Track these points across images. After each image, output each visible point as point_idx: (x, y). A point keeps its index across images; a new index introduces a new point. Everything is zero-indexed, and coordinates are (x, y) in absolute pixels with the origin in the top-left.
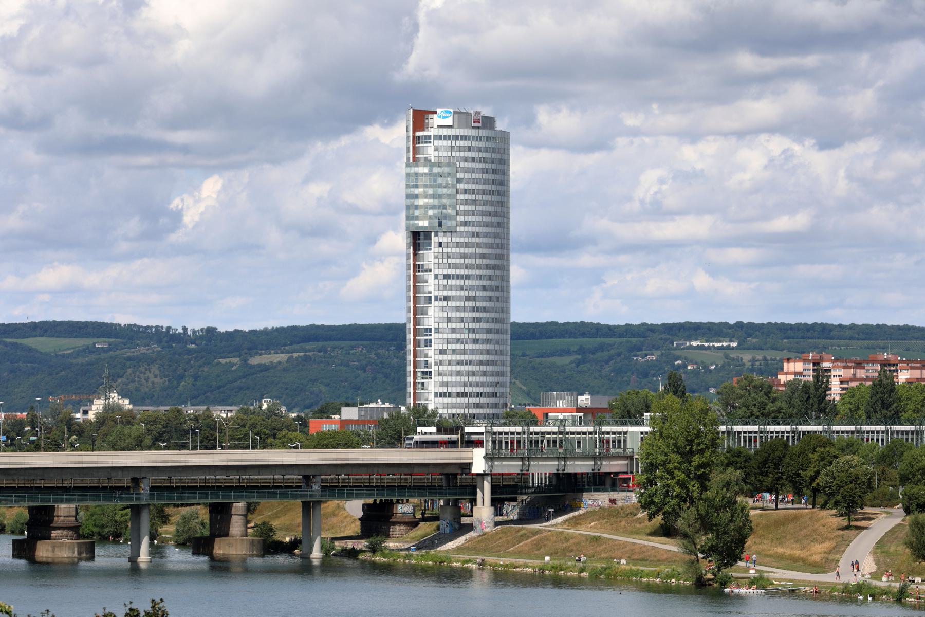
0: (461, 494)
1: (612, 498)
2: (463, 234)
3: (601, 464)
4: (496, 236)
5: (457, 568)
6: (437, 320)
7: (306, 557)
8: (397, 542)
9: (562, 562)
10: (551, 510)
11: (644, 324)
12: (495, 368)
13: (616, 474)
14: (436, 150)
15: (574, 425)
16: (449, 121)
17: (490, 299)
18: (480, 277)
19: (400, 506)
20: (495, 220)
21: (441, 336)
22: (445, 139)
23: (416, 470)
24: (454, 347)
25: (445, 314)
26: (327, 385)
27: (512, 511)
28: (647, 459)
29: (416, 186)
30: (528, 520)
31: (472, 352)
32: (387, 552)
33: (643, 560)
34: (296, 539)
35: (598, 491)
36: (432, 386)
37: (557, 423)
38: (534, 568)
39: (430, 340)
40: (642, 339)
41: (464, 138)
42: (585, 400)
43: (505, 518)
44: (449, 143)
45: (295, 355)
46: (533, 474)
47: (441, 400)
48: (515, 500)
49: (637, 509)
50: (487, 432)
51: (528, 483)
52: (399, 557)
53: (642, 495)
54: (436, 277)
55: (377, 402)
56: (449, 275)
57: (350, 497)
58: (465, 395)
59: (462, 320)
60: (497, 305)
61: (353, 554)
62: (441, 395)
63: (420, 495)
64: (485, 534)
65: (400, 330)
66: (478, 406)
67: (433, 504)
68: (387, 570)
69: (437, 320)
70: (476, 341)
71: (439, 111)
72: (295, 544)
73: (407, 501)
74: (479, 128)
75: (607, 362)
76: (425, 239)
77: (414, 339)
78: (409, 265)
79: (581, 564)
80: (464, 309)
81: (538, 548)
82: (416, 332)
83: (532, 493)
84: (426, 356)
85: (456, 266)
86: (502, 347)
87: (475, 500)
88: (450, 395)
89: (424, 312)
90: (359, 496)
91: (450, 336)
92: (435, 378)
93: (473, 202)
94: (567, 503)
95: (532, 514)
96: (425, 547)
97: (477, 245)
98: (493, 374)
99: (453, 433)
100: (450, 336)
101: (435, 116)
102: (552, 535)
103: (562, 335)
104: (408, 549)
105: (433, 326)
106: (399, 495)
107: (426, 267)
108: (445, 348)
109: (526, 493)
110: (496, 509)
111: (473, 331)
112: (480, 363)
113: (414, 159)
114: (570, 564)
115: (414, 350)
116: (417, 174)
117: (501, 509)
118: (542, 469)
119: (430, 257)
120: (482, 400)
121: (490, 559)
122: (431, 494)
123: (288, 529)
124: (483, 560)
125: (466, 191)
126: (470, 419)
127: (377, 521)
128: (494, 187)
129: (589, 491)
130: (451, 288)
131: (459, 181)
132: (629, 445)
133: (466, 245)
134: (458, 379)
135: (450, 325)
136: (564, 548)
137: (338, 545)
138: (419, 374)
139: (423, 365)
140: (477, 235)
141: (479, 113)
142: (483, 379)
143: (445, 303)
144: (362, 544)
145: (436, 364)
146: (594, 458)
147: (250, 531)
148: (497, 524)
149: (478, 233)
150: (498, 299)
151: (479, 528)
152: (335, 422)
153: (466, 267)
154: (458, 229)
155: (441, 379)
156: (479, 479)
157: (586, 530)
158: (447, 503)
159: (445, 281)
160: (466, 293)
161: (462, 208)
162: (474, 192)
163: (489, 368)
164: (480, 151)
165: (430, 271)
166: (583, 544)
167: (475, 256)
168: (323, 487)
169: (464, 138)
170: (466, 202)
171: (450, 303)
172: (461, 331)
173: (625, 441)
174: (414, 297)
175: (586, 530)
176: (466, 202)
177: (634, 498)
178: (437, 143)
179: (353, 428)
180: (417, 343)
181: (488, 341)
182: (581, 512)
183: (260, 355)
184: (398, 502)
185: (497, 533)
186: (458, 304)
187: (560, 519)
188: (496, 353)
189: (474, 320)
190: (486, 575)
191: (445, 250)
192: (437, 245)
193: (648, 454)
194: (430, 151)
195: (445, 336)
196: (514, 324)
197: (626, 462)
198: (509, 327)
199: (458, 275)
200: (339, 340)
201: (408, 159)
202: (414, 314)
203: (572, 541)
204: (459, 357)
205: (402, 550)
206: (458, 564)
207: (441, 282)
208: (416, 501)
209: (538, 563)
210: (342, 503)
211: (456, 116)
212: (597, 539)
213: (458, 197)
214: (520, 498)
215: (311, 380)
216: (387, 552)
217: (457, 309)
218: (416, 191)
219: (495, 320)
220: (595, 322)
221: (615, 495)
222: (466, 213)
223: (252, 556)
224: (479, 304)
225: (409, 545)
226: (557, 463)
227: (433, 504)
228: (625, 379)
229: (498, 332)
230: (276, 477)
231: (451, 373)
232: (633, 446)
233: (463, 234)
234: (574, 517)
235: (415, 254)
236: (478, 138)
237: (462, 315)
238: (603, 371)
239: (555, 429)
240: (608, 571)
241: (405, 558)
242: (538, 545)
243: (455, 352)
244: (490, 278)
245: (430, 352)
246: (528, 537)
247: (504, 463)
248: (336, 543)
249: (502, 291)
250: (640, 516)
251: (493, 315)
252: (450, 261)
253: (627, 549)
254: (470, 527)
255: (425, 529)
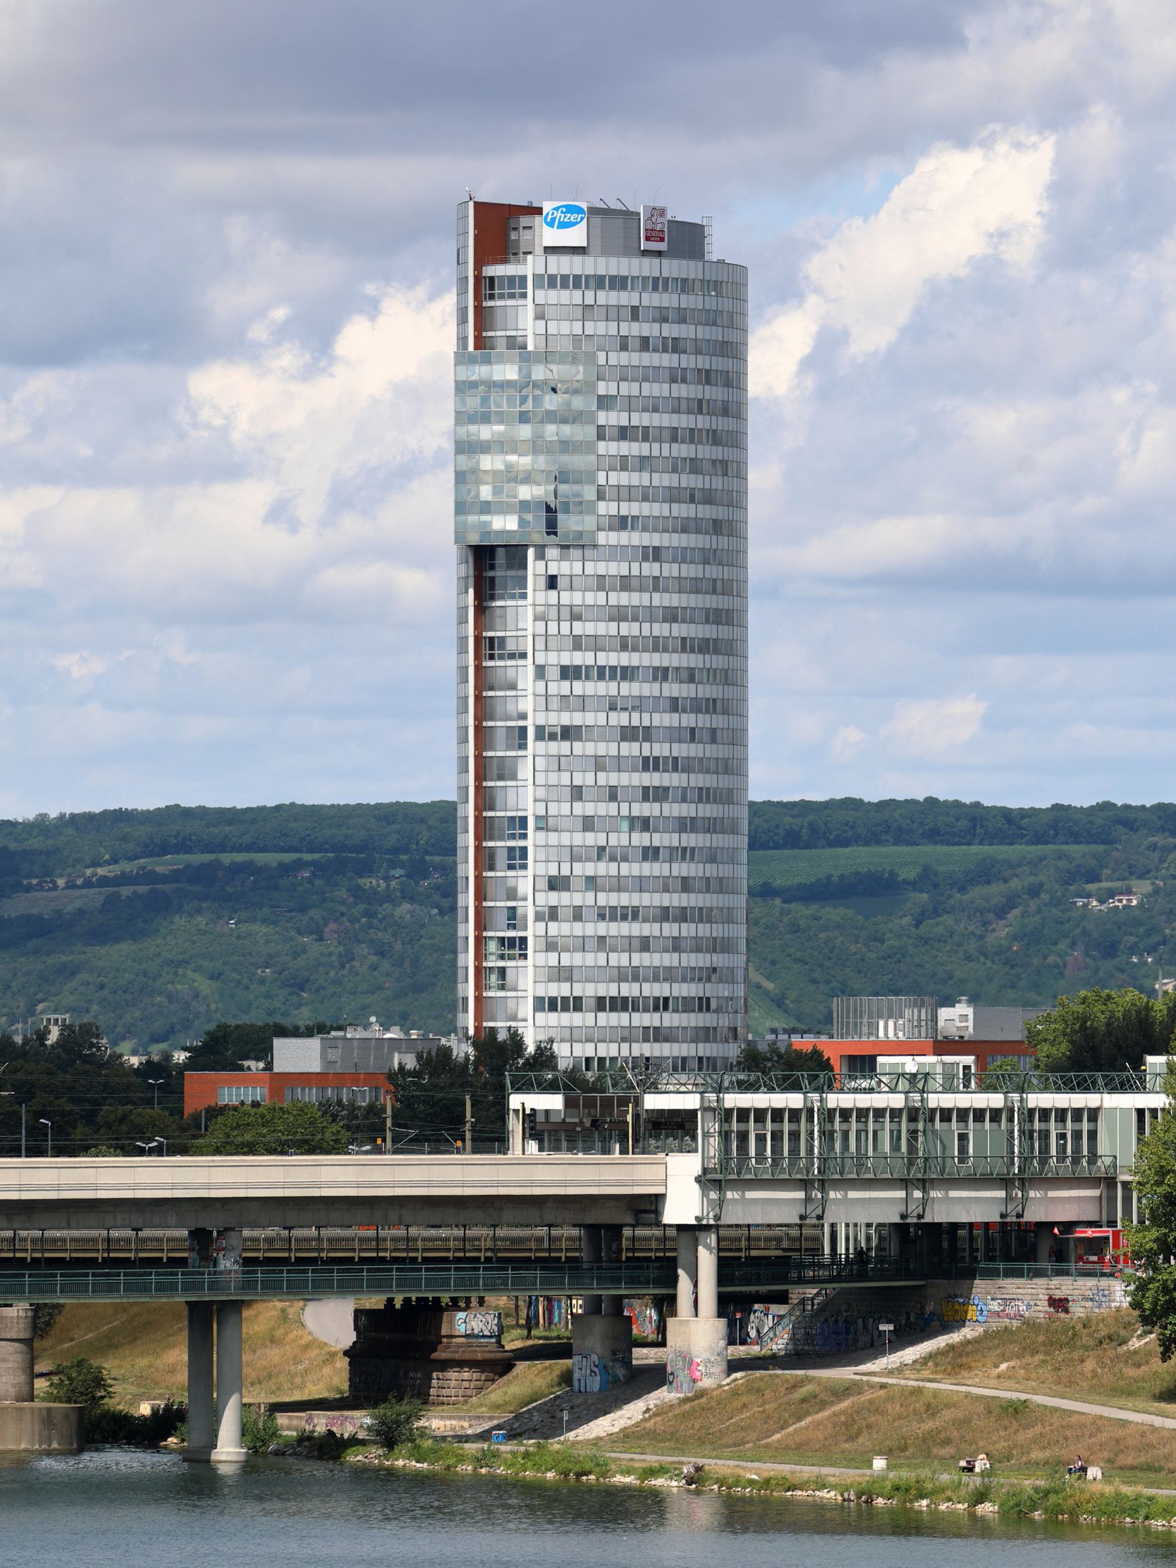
0: (633, 1282)
1: (1058, 1294)
2: (615, 553)
3: (1025, 1199)
4: (707, 557)
5: (626, 1489)
6: (541, 792)
7: (199, 1459)
8: (456, 1417)
9: (925, 1473)
10: (886, 1327)
11: (1107, 806)
12: (704, 930)
13: (1068, 1226)
14: (540, 316)
15: (948, 1089)
16: (576, 236)
17: (692, 735)
18: (661, 674)
19: (461, 1315)
20: (706, 512)
21: (553, 838)
22: (564, 286)
23: (508, 1214)
24: (590, 869)
25: (565, 778)
26: (215, 976)
27: (773, 1330)
28: (1159, 1183)
29: (485, 418)
30: (820, 1355)
31: (641, 884)
32: (429, 1443)
33: (1149, 1468)
34: (168, 1408)
35: (1018, 1274)
36: (529, 978)
37: (903, 1085)
38: (843, 1489)
39: (524, 850)
40: (1101, 848)
41: (619, 283)
42: (957, 1017)
43: (755, 1350)
44: (577, 296)
45: (126, 891)
46: (833, 1226)
47: (553, 1018)
48: (782, 1298)
49: (1127, 1325)
50: (705, 1109)
51: (817, 1250)
52: (461, 1459)
53: (1142, 1287)
54: (540, 671)
55: (367, 1026)
56: (577, 669)
57: (322, 1289)
58: (619, 1004)
59: (613, 794)
60: (711, 751)
61: (330, 1448)
62: (553, 1005)
63: (519, 1284)
64: (701, 1394)
65: (443, 816)
66: (658, 1035)
67: (549, 1311)
68: (436, 1496)
69: (541, 792)
70: (650, 854)
71: (547, 207)
72: (166, 1422)
73: (481, 1301)
74: (659, 254)
75: (1001, 912)
76: (510, 566)
77: (478, 848)
78: (463, 640)
79: (978, 1480)
80: (619, 763)
81: (852, 1434)
82: (484, 829)
83: (831, 1280)
84: (512, 894)
85: (596, 644)
86: (725, 871)
87: (672, 1300)
88: (577, 1004)
89: (507, 771)
90: (345, 1288)
91: (578, 839)
92: (536, 958)
93: (644, 463)
94: (930, 1308)
95: (837, 1336)
96: (533, 1432)
97: (656, 585)
98: (698, 946)
99: (601, 1112)
100: (578, 839)
101: (537, 218)
102: (890, 1399)
103: (874, 839)
104: (484, 1436)
105: (531, 810)
106: (461, 1284)
107: (511, 646)
108: (566, 871)
109: (814, 1281)
110: (731, 1325)
111: (645, 824)
112: (664, 914)
113: (480, 343)
114: (945, 1478)
115: (478, 878)
116: (491, 385)
117: (744, 1323)
118: (860, 1213)
119: (524, 615)
120: (669, 1019)
121: (720, 1466)
122: (547, 1283)
123: (146, 1385)
124: (698, 1469)
125: (624, 433)
126: (650, 1073)
127: (396, 1358)
128: (702, 422)
129: (992, 1274)
130: (583, 703)
131: (605, 402)
132: (1103, 1147)
133: (625, 584)
134: (601, 959)
135: (578, 808)
136: (929, 1436)
137: (289, 1425)
138: (492, 946)
139: (502, 919)
140: (656, 554)
141: (662, 212)
142: (669, 959)
143: (565, 747)
144: (357, 1422)
145: (539, 917)
146: (1005, 1182)
147: (41, 1385)
148: (733, 1366)
149: (657, 550)
150: (713, 736)
151: (682, 1377)
152: (254, 1082)
153: (625, 645)
154: (602, 538)
155: (552, 959)
156: (685, 1238)
157: (990, 1384)
158: (594, 1306)
159: (566, 684)
160: (623, 719)
161: (615, 478)
162: (645, 434)
163: (687, 930)
164: (664, 320)
165: (523, 656)
166: (975, 1422)
167: (650, 614)
168: (247, 1262)
169: (619, 283)
170: (623, 464)
171: (578, 747)
172: (610, 824)
173: (1093, 1135)
174: (478, 728)
175: (990, 1384)
176: (623, 464)
177: (1119, 1294)
178: (542, 296)
179: (311, 1096)
180: (486, 859)
181: (685, 854)
182: (967, 1333)
183: (28, 889)
184: (455, 1305)
185: (735, 1393)
186: (602, 749)
187: (910, 1354)
188: (708, 885)
189: (647, 794)
190: (704, 1511)
191: (566, 598)
192: (542, 582)
193: (1162, 1172)
194: (523, 319)
195: (566, 838)
196: (756, 809)
197: (1096, 1193)
198: (745, 812)
199: (601, 669)
200: (249, 848)
201: (462, 340)
202: (479, 778)
203: (947, 1415)
204: (603, 899)
205: (467, 1439)
206: (629, 1480)
207: (553, 688)
208: (502, 1300)
209: (852, 1475)
210: (293, 1307)
211: (597, 220)
212: (1017, 1410)
213: (602, 447)
214: (797, 1293)
215: (169, 963)
216: (429, 1443)
217: (599, 764)
218: (485, 432)
219: (704, 795)
220: (967, 800)
221: (1064, 1286)
222: (625, 494)
223: (49, 1453)
224: (660, 749)
225: (487, 1426)
226: (901, 1194)
227: (549, 1311)
228: (1051, 959)
229: (711, 826)
230: (115, 1233)
231: (582, 945)
232: (1118, 1147)
233: (615, 553)
234: (951, 1348)
235: (481, 609)
236: (657, 284)
237: (613, 778)
238: (990, 939)
239: (897, 1101)
240: (1053, 1498)
241: (479, 1461)
242: (850, 1427)
243: (592, 882)
244: (691, 676)
245: (525, 885)
246: (823, 1405)
247: (750, 1195)
248: (282, 1419)
249: (725, 712)
250: (1135, 1344)
251: (698, 780)
252: (578, 629)
253: (1103, 1437)
254: (657, 1376)
255: (531, 1380)
